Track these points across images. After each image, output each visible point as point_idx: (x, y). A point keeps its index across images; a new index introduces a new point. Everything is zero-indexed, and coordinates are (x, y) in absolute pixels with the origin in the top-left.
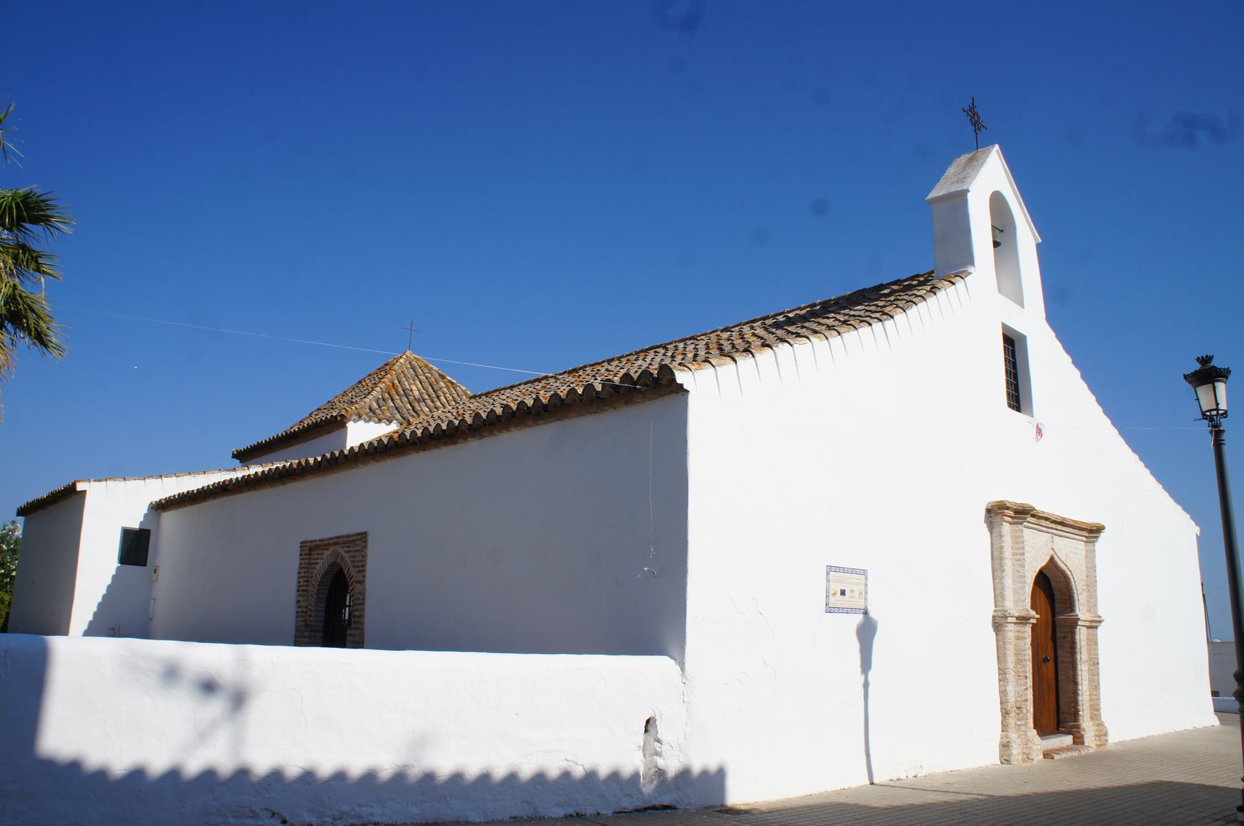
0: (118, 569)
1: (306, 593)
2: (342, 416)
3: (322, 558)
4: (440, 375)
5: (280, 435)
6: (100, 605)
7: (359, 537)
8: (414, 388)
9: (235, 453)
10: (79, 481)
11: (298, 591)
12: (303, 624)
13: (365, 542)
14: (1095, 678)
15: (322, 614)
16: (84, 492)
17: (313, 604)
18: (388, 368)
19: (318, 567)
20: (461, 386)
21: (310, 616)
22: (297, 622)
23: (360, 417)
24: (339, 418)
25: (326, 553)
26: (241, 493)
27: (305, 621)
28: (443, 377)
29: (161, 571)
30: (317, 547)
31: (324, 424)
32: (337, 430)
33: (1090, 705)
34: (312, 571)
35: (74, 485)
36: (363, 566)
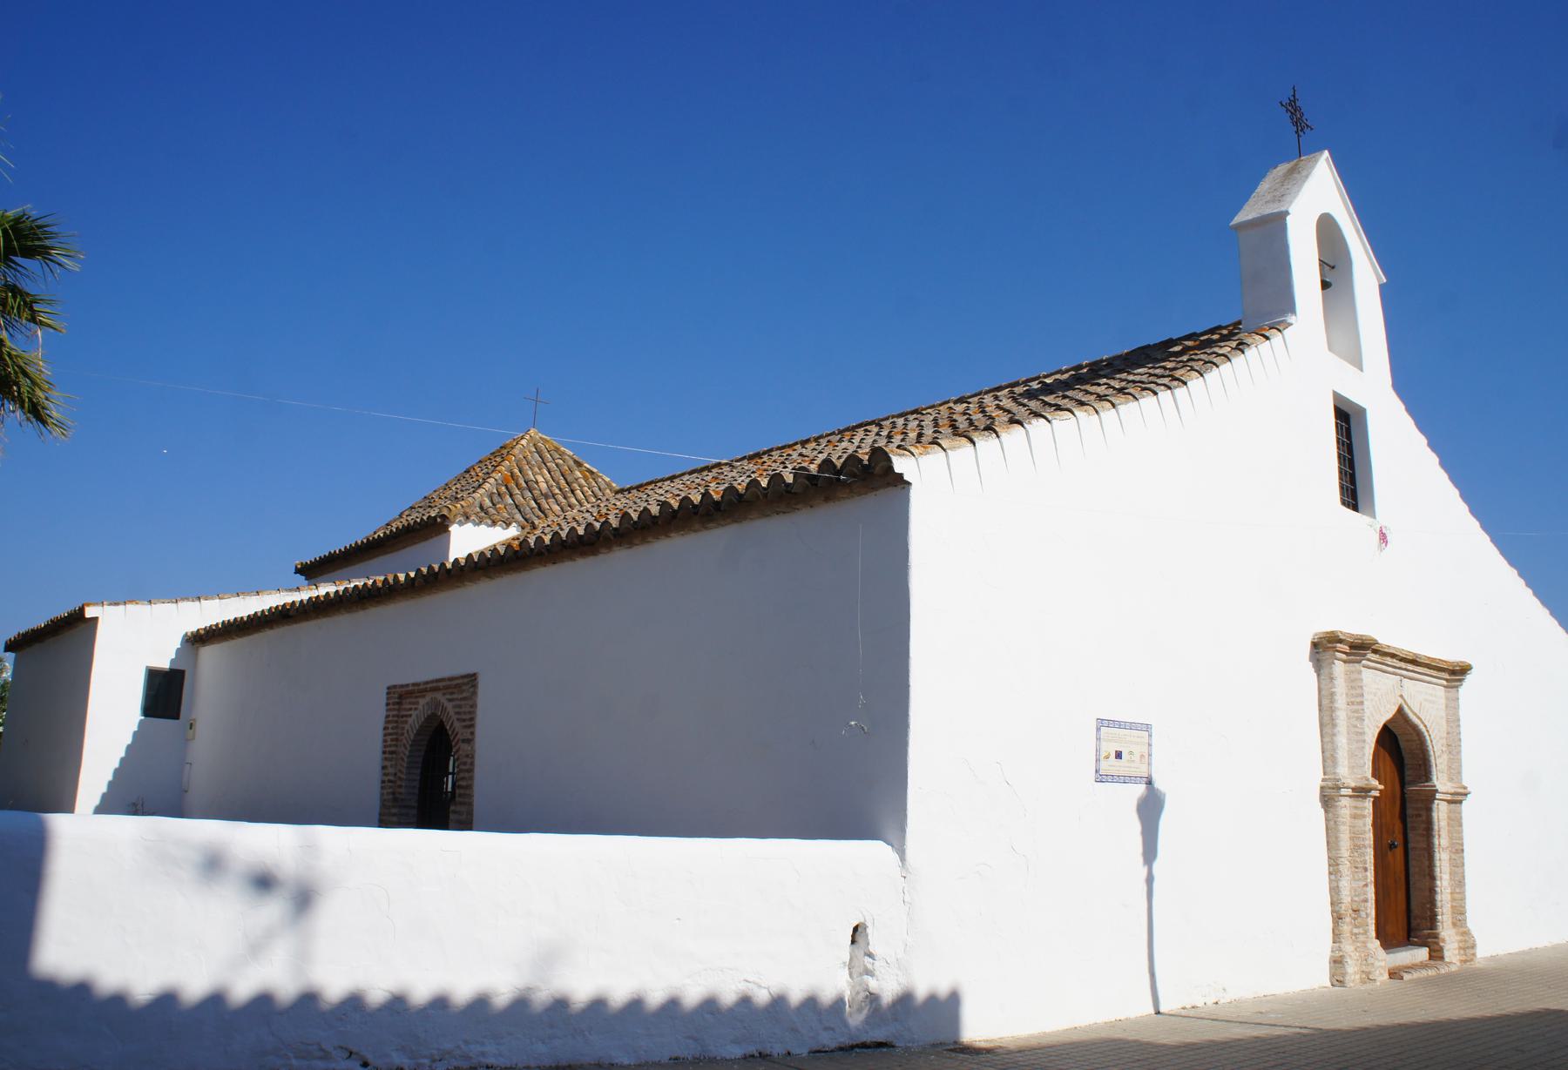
0: (141, 723)
1: (394, 756)
2: (444, 517)
3: (416, 709)
5: (359, 542)
7: (466, 680)
9: (299, 566)
10: (88, 605)
11: (384, 753)
12: (391, 796)
15: (417, 784)
16: (95, 620)
19: (410, 720)
20: (604, 477)
21: (400, 786)
22: (382, 794)
23: (468, 518)
24: (439, 520)
25: (422, 701)
27: (393, 793)
28: (579, 464)
29: (199, 726)
30: (410, 694)
31: (418, 527)
33: (1452, 907)
35: (82, 610)
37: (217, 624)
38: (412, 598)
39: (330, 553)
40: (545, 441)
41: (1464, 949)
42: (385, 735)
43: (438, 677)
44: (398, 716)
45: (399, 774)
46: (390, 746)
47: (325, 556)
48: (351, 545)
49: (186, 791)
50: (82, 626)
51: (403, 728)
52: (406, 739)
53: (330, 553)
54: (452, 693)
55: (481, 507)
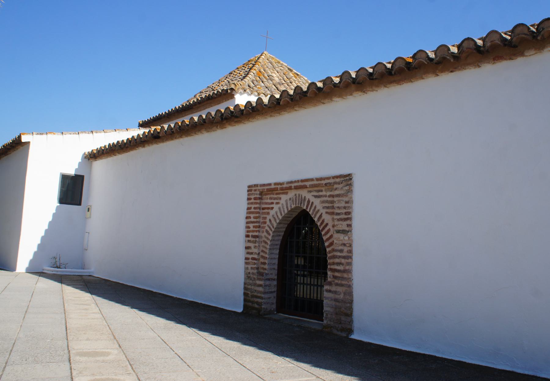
0: (58, 208)
1: (257, 239)
2: (232, 89)
3: (277, 203)
4: (289, 69)
5: (177, 107)
6: (43, 238)
7: (338, 180)
8: (274, 75)
9: (141, 123)
10: (24, 134)
11: (247, 236)
12: (256, 271)
13: (350, 185)
15: (276, 261)
16: (28, 143)
17: (268, 252)
19: (272, 212)
20: (304, 77)
21: (264, 263)
22: (246, 269)
23: (245, 91)
24: (229, 91)
25: (284, 198)
26: (172, 140)
27: (258, 268)
28: (291, 70)
29: (93, 210)
30: (271, 191)
31: (215, 96)
32: (226, 101)
34: (265, 216)
35: (20, 137)
36: (349, 213)
37: (105, 146)
38: (271, 116)
39: (159, 114)
40: (273, 58)
42: (247, 223)
43: (304, 177)
44: (260, 208)
45: (262, 254)
46: (253, 231)
47: (156, 116)
48: (172, 109)
49: (87, 250)
50: (21, 148)
51: (265, 218)
52: (268, 226)
53: (159, 114)
54: (319, 191)
55: (249, 86)
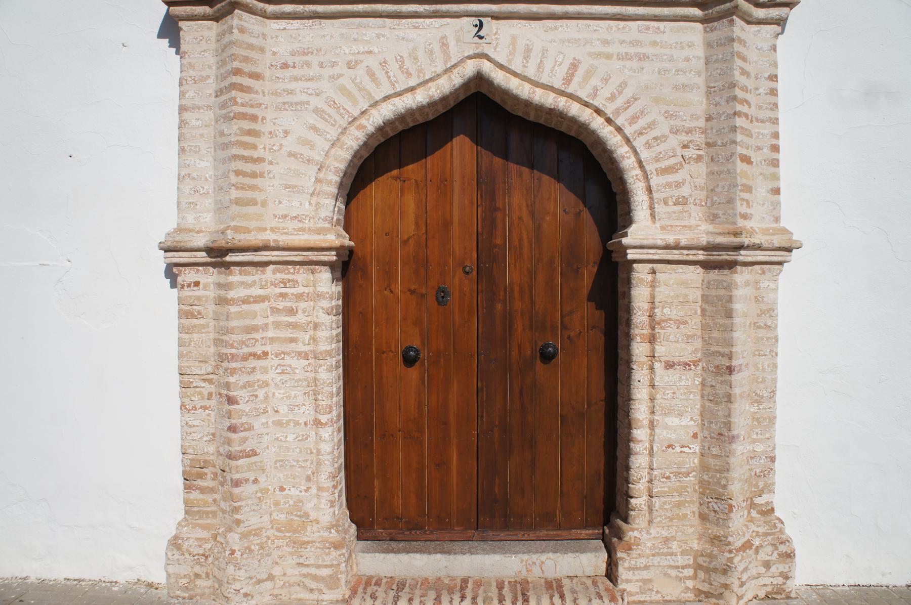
14: (721, 411)
18: (233, 57)
33: (701, 482)
41: (707, 570)
